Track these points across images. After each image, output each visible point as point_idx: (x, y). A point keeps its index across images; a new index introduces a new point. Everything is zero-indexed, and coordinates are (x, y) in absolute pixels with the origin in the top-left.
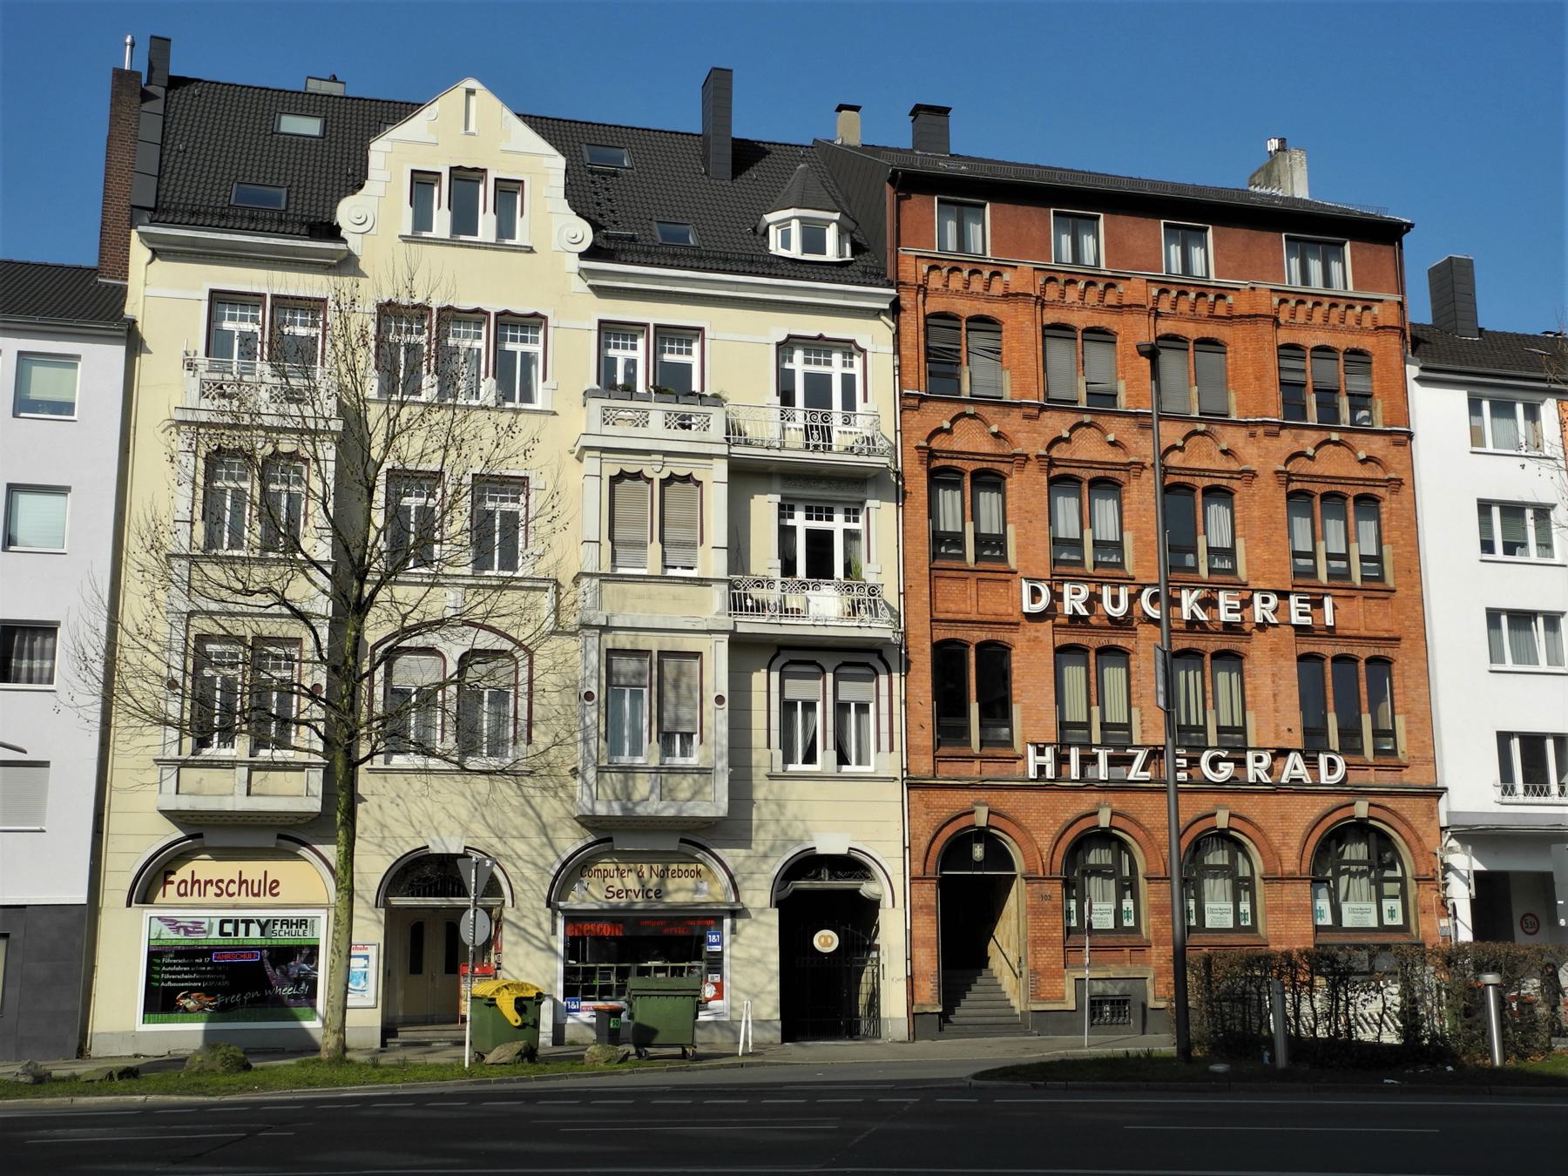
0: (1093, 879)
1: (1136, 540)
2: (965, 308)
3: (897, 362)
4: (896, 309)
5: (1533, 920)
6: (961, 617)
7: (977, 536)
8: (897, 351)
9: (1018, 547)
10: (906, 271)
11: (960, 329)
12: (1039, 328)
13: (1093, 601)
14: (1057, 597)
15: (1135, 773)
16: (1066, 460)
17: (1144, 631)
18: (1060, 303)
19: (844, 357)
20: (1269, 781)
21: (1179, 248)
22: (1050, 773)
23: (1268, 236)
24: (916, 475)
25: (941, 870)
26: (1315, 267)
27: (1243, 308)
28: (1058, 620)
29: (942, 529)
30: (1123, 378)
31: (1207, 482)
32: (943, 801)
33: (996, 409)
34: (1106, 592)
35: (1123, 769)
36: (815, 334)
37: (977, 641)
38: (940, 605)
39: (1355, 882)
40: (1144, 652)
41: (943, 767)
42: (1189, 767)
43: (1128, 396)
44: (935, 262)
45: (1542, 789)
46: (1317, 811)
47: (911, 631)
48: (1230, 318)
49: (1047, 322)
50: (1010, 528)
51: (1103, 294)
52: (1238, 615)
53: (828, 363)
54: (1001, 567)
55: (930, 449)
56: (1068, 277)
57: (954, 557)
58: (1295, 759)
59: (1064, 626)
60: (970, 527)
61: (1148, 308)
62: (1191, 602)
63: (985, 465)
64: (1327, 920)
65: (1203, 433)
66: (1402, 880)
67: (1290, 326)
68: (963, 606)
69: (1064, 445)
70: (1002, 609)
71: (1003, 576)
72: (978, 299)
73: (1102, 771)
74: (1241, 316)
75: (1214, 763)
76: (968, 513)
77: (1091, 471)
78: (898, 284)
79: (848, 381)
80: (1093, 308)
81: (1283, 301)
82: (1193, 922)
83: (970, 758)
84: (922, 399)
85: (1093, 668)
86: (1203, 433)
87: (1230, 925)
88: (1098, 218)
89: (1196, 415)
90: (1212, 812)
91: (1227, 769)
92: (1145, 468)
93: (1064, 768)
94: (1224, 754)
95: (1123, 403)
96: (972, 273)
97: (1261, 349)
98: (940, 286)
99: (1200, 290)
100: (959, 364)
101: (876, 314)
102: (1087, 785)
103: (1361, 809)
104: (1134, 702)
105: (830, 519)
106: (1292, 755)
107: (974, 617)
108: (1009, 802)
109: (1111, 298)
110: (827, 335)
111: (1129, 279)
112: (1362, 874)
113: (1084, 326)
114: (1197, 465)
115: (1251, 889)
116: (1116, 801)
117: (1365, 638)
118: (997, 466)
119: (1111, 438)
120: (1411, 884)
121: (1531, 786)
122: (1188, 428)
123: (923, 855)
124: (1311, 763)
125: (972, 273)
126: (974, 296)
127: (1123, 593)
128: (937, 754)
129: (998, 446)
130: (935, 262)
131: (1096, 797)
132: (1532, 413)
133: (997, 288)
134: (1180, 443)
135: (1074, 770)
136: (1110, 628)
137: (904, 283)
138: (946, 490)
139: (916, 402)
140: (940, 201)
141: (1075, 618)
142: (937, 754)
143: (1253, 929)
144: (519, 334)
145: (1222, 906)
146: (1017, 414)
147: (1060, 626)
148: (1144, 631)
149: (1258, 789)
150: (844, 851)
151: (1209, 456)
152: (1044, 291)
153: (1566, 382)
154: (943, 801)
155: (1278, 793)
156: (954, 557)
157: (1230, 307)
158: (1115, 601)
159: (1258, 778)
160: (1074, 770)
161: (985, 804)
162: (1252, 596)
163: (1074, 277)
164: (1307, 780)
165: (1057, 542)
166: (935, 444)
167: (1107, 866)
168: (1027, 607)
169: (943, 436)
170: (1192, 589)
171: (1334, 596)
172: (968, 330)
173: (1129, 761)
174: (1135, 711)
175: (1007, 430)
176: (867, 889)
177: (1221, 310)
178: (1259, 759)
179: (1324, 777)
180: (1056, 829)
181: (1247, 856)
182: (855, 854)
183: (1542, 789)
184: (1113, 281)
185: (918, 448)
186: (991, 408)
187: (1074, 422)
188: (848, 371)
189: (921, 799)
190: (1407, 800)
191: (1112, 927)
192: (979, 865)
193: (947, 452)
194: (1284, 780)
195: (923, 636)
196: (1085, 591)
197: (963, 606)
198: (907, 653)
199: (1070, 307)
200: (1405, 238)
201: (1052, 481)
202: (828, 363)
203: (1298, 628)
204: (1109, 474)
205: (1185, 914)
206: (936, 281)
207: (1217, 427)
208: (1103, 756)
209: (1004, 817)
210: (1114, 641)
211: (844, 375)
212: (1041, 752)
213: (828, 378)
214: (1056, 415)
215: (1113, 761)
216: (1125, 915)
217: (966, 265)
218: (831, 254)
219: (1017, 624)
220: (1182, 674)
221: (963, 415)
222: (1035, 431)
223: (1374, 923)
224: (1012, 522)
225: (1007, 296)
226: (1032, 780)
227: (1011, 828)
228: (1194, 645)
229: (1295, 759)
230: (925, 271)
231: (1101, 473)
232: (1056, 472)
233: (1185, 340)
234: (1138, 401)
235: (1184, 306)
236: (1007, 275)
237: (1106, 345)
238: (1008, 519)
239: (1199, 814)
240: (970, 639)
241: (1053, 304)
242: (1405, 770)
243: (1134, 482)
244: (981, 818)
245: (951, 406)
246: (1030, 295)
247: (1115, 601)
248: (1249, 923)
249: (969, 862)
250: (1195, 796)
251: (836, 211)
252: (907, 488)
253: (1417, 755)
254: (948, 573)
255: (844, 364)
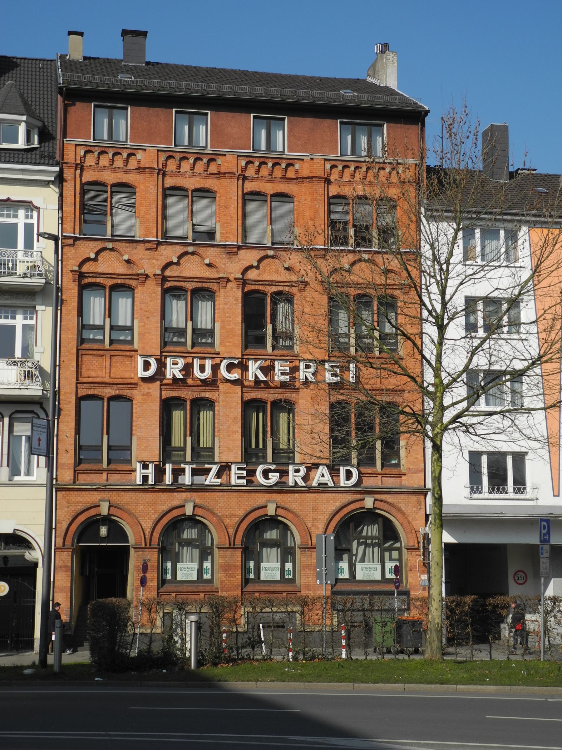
0: (185, 548)
1: (222, 328)
2: (110, 178)
3: (60, 215)
4: (60, 180)
5: (523, 575)
6: (98, 380)
7: (194, 330)
8: (61, 208)
9: (140, 334)
10: (68, 155)
11: (107, 192)
12: (160, 190)
13: (187, 369)
14: (161, 365)
15: (211, 479)
16: (175, 277)
17: (223, 387)
18: (178, 172)
19: (27, 212)
20: (304, 484)
21: (366, 138)
22: (151, 481)
23: (327, 122)
24: (70, 289)
25: (78, 542)
26: (363, 141)
27: (305, 173)
28: (165, 382)
29: (199, 327)
30: (219, 221)
31: (274, 289)
32: (79, 499)
33: (128, 245)
34: (197, 363)
35: (203, 478)
36: (5, 198)
37: (109, 395)
38: (85, 373)
39: (369, 550)
40: (223, 401)
41: (81, 477)
42: (248, 475)
43: (221, 233)
44: (89, 148)
45: (477, 488)
46: (338, 504)
47: (63, 391)
48: (297, 179)
49: (167, 185)
50: (136, 322)
51: (208, 165)
52: (288, 377)
53: (16, 216)
54: (127, 347)
55: (244, 280)
56: (182, 155)
57: (206, 345)
58: (323, 470)
59: (168, 385)
60: (190, 324)
61: (237, 174)
62: (255, 367)
63: (119, 281)
64: (346, 575)
65: (273, 257)
66: (399, 549)
67: (339, 184)
68: (100, 373)
69: (175, 267)
70: (127, 375)
71: (128, 353)
72: (119, 172)
73: (187, 479)
74: (303, 178)
75: (265, 474)
76: (107, 312)
77: (193, 284)
78: (63, 163)
79: (29, 228)
80: (200, 175)
81: (333, 167)
82: (252, 576)
83: (100, 471)
84: (76, 239)
85: (188, 412)
86: (273, 257)
87: (278, 578)
88: (284, 119)
89: (269, 245)
90: (264, 504)
91: (274, 477)
92: (230, 281)
93: (180, 478)
94: (273, 467)
95: (219, 239)
96: (115, 154)
97: (316, 199)
98: (93, 164)
99: (196, 156)
100: (106, 215)
101: (47, 183)
102: (176, 487)
103: (369, 503)
104: (216, 434)
105: (14, 318)
106: (321, 467)
107: (107, 380)
108: (123, 499)
109: (213, 168)
110: (13, 198)
111: (225, 155)
112: (373, 545)
113: (193, 188)
114: (268, 278)
115: (293, 555)
116: (198, 498)
117: (110, 384)
118: (127, 282)
119: (207, 261)
120: (404, 551)
121: (475, 487)
122: (262, 253)
123: (63, 534)
124: (333, 471)
125: (115, 154)
126: (118, 170)
127: (208, 363)
128: (77, 468)
129: (129, 268)
130: (89, 148)
131: (184, 495)
132: (512, 236)
133: (133, 164)
134: (255, 264)
135: (168, 478)
136: (201, 386)
137: (66, 163)
138: (95, 297)
139: (71, 241)
140: (341, 123)
141: (175, 380)
142: (77, 468)
143: (293, 581)
144: (12, 213)
145: (273, 566)
146: (142, 247)
147: (165, 385)
148: (223, 387)
149: (295, 490)
150: (11, 531)
151: (277, 271)
152: (165, 165)
153: (560, 217)
154: (79, 499)
155: (311, 492)
156: (206, 345)
157: (297, 172)
158: (202, 369)
159: (296, 483)
160: (168, 478)
161: (106, 501)
162: (193, 361)
163: (186, 155)
164: (331, 484)
165: (166, 330)
166: (85, 269)
167: (195, 540)
168: (141, 373)
169: (91, 263)
170: (256, 360)
171: (200, 358)
172: (112, 192)
173: (207, 472)
174: (216, 439)
175: (134, 258)
176: (30, 556)
177: (291, 173)
178: (297, 471)
179: (343, 482)
180: (156, 516)
181: (209, 531)
182: (18, 533)
183: (477, 488)
184: (214, 157)
185: (72, 271)
186: (124, 244)
187: (182, 251)
188: (29, 221)
189: (64, 497)
190: (403, 497)
191: (195, 579)
192: (103, 540)
193: (92, 273)
194: (315, 484)
195: (71, 393)
196: (181, 362)
197: (100, 373)
198: (59, 404)
199: (184, 175)
200: (427, 119)
201: (165, 292)
202: (16, 216)
203: (330, 384)
204: (205, 285)
205: (246, 570)
206: (90, 160)
207: (281, 253)
208: (188, 469)
209: (120, 509)
210: (203, 395)
211: (26, 224)
212: (145, 467)
213: (15, 226)
214: (169, 247)
215: (194, 472)
216: (204, 571)
217: (111, 149)
218: (21, 144)
219: (136, 384)
220: (254, 415)
221: (104, 249)
222: (154, 259)
223: (378, 577)
224: (137, 318)
225: (139, 169)
226: (168, 485)
227: (125, 516)
228: (259, 396)
229: (323, 470)
230: (82, 154)
231: (200, 285)
232: (168, 285)
233: (265, 195)
234: (227, 237)
235: (264, 171)
236: (140, 155)
237: (209, 200)
238: (135, 316)
239: (256, 506)
240: (103, 395)
241: (172, 173)
242: (403, 477)
243: (222, 290)
244: (104, 510)
245: (96, 243)
246: (154, 169)
247: (202, 369)
248: (291, 577)
249: (96, 537)
250: (253, 494)
251: (23, 115)
252: (64, 297)
253: (411, 467)
254: (91, 352)
255: (27, 217)
